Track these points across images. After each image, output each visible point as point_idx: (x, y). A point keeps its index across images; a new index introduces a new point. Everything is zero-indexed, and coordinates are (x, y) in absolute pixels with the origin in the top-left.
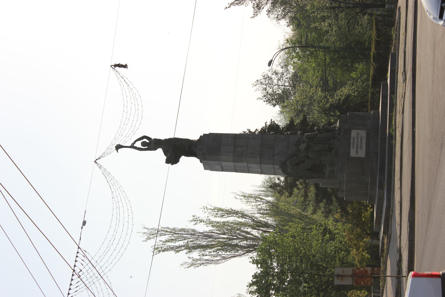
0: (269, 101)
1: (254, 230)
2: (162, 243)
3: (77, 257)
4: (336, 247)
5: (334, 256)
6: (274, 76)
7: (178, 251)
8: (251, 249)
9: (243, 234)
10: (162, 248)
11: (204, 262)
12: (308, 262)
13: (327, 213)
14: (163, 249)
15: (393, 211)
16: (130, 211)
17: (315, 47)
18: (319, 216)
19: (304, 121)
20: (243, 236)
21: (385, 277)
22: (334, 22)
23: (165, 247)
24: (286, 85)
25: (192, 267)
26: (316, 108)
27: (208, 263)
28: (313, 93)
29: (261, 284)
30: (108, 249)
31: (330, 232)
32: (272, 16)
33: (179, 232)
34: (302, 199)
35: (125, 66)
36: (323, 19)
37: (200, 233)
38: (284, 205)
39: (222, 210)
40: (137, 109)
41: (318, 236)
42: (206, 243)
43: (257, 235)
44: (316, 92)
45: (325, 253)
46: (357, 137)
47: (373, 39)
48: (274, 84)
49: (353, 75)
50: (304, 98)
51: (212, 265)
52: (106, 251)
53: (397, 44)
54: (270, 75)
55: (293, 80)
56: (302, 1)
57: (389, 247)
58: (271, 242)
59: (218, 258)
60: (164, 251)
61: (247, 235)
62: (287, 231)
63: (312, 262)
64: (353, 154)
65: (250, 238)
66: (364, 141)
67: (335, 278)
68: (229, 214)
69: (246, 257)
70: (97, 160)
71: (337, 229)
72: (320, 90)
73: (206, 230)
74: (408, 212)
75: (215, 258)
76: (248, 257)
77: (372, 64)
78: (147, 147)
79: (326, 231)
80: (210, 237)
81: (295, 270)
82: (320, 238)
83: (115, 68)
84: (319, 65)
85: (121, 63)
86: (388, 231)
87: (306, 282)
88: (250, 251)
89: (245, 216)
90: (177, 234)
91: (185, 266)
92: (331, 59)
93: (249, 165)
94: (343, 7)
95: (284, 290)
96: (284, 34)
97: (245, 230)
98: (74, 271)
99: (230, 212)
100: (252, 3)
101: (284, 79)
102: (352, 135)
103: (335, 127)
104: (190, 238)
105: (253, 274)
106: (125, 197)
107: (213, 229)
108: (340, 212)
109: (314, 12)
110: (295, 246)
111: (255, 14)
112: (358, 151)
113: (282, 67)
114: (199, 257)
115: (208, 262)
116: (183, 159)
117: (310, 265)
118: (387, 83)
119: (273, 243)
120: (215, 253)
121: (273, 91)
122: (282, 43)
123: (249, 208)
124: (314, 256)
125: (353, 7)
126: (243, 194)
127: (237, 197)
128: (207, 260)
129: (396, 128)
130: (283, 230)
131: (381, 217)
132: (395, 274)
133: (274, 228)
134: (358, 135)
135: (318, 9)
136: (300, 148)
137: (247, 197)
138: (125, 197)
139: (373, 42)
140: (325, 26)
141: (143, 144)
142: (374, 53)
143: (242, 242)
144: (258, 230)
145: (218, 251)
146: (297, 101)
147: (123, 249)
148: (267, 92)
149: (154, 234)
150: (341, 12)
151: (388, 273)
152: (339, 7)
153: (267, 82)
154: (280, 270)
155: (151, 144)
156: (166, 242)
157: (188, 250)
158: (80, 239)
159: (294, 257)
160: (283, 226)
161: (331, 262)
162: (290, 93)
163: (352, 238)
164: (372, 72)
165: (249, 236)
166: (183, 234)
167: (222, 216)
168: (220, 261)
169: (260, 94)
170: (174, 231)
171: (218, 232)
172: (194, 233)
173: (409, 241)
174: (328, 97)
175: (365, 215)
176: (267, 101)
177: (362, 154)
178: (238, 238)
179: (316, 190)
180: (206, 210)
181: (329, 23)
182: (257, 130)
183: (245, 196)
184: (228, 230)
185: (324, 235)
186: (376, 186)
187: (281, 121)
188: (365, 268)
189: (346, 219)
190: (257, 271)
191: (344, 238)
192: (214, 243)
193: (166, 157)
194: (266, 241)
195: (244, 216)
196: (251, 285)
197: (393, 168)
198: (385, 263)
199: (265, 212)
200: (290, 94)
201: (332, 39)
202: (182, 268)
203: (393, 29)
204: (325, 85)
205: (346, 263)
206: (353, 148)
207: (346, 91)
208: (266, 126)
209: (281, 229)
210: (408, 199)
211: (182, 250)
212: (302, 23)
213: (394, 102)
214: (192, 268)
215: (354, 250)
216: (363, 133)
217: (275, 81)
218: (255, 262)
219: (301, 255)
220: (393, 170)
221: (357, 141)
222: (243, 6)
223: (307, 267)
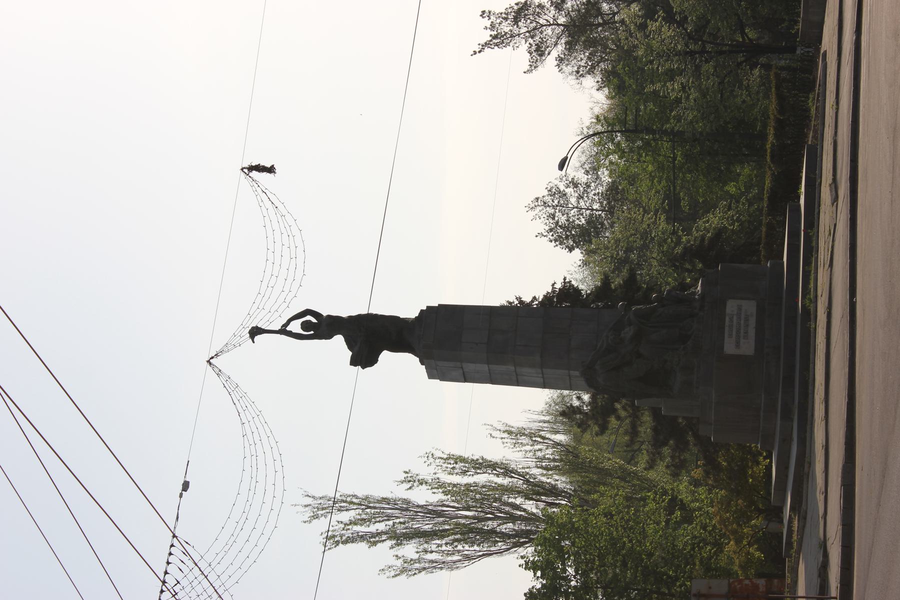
0: (559, 240)
1: (528, 502)
3: (170, 554)
4: (695, 537)
5: (691, 556)
6: (569, 191)
7: (375, 543)
9: (507, 509)
10: (341, 536)
11: (427, 565)
12: (637, 567)
14: (344, 538)
15: (811, 464)
16: (278, 463)
17: (653, 132)
19: (631, 282)
20: (505, 513)
22: (693, 82)
23: (348, 534)
24: (595, 207)
26: (655, 255)
27: (435, 567)
28: (649, 225)
30: (233, 539)
31: (683, 506)
32: (568, 69)
33: (377, 505)
35: (271, 170)
36: (671, 75)
37: (418, 506)
38: (590, 451)
39: (463, 460)
40: (293, 256)
41: (659, 514)
42: (430, 526)
43: (535, 511)
44: (655, 223)
47: (772, 117)
48: (570, 206)
49: (731, 188)
50: (632, 235)
51: (444, 571)
52: (230, 543)
54: (562, 188)
57: (802, 538)
58: (562, 526)
59: (456, 558)
60: (345, 542)
62: (595, 504)
63: (646, 567)
64: (729, 348)
65: (520, 518)
66: (753, 322)
68: (478, 468)
70: (212, 358)
71: (697, 500)
73: (431, 501)
74: (841, 466)
75: (450, 558)
76: (516, 555)
79: (675, 503)
80: (440, 514)
82: (663, 519)
83: (251, 174)
84: (661, 168)
88: (522, 545)
89: (511, 472)
90: (372, 507)
91: (388, 574)
94: (711, 52)
96: (591, 105)
97: (510, 500)
98: (164, 582)
99: (480, 464)
100: (528, 44)
101: (591, 195)
102: (728, 310)
103: (694, 293)
104: (397, 518)
105: (527, 591)
106: (269, 434)
107: (445, 498)
108: (704, 465)
109: (651, 62)
110: (611, 534)
111: (533, 66)
112: (739, 343)
113: (587, 173)
114: (416, 556)
115: (435, 565)
116: (386, 356)
118: (800, 206)
119: (566, 528)
120: (449, 548)
121: (568, 220)
122: (588, 124)
124: (650, 555)
126: (507, 428)
127: (495, 434)
128: (432, 561)
129: (816, 297)
130: (586, 501)
131: (787, 476)
133: (568, 496)
134: (741, 311)
137: (515, 434)
140: (673, 89)
141: (306, 326)
143: (505, 526)
144: (537, 501)
145: (456, 544)
146: (617, 241)
147: (264, 538)
148: (557, 223)
150: (707, 61)
152: (703, 51)
153: (556, 202)
155: (321, 327)
156: (351, 523)
157: (394, 542)
158: (177, 518)
160: (589, 492)
161: (685, 567)
162: (602, 224)
163: (728, 519)
164: (768, 183)
165: (519, 513)
166: (384, 508)
167: (464, 473)
168: (458, 564)
169: (542, 226)
170: (365, 503)
171: (457, 505)
172: (406, 506)
174: (680, 233)
175: (753, 472)
176: (556, 240)
177: (748, 348)
178: (496, 518)
180: (431, 460)
182: (534, 298)
184: (476, 500)
185: (671, 513)
188: (754, 580)
189: (715, 480)
190: (534, 583)
191: (711, 519)
192: (447, 527)
193: (351, 353)
194: (552, 524)
197: (811, 376)
199: (552, 464)
202: (383, 577)
203: (811, 96)
206: (730, 336)
208: (554, 291)
209: (583, 499)
210: (842, 440)
211: (383, 541)
212: (627, 84)
213: (814, 244)
214: (403, 577)
215: (732, 542)
216: (750, 307)
217: (573, 200)
218: (531, 566)
219: (624, 552)
222: (509, 48)
223: (636, 577)
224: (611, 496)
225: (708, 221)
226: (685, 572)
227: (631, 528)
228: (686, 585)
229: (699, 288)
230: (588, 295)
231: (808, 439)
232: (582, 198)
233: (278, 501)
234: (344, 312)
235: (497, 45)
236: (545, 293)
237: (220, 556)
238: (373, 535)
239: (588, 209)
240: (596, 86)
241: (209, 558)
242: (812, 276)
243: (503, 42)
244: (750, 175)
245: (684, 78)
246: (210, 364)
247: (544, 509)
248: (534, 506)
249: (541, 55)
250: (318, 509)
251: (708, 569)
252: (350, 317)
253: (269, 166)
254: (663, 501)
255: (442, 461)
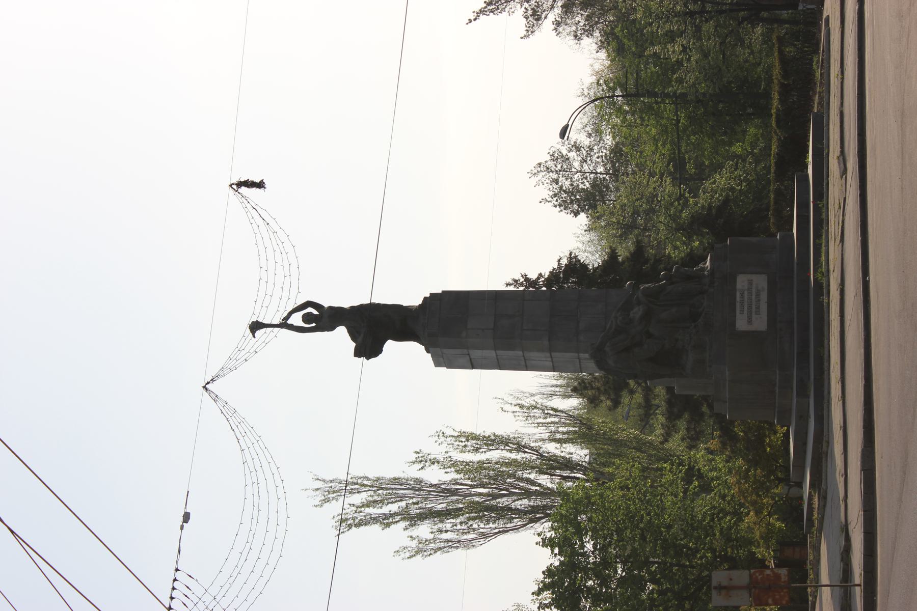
0: (564, 205)
1: (543, 477)
2: (354, 509)
3: (174, 589)
4: (714, 507)
5: (711, 527)
6: (572, 155)
8: (538, 516)
9: (521, 484)
10: (354, 519)
11: (442, 545)
12: (656, 540)
13: (692, 439)
14: (357, 521)
15: (829, 443)
16: (280, 489)
17: (655, 95)
18: (676, 444)
19: (638, 253)
20: (520, 489)
21: (816, 587)
22: (694, 44)
23: (360, 516)
24: (598, 171)
25: (419, 557)
26: (662, 219)
27: (450, 547)
29: (562, 586)
30: (237, 570)
31: (700, 476)
32: (566, 29)
33: (389, 486)
34: (641, 411)
35: (260, 185)
36: (671, 37)
37: (431, 485)
38: (603, 422)
39: (475, 437)
40: (287, 274)
41: (677, 485)
42: (444, 505)
43: (550, 485)
44: (661, 185)
45: (692, 519)
46: (750, 289)
47: (776, 81)
48: (573, 170)
49: (737, 149)
50: (637, 200)
51: (460, 550)
52: (234, 575)
53: (825, 94)
54: (564, 152)
55: (612, 162)
56: (624, 1)
57: (823, 517)
58: (578, 502)
59: (471, 536)
60: (358, 525)
61: (529, 487)
62: (611, 477)
63: (665, 540)
64: (741, 324)
65: (536, 493)
66: (764, 296)
67: (714, 593)
68: (490, 445)
69: (528, 531)
70: (208, 383)
71: (715, 469)
72: (668, 180)
74: (860, 450)
75: (465, 537)
76: (533, 531)
77: (775, 132)
78: (314, 325)
79: (692, 473)
80: (454, 493)
81: (629, 556)
83: (240, 190)
84: (665, 131)
85: (251, 179)
86: (820, 484)
87: (653, 581)
88: (536, 520)
89: (525, 447)
90: (386, 488)
91: (403, 555)
92: (689, 118)
93: (527, 354)
94: (710, 12)
95: (608, 598)
96: (591, 61)
97: (525, 475)
99: (494, 440)
100: (523, 9)
101: (594, 158)
102: (739, 285)
103: (703, 269)
104: (412, 498)
106: (270, 460)
107: (458, 476)
108: (720, 436)
109: (651, 24)
110: (628, 507)
111: (530, 31)
112: (752, 318)
113: (589, 135)
114: (431, 536)
115: (451, 545)
117: (662, 547)
118: (808, 175)
119: (583, 503)
120: (464, 527)
121: (572, 185)
122: (587, 84)
123: (530, 431)
124: (669, 527)
125: (731, 11)
126: (519, 402)
128: (448, 541)
129: (828, 271)
130: (602, 474)
132: (839, 575)
133: (584, 470)
134: (751, 286)
135: (658, 17)
136: (631, 315)
137: (528, 410)
138: (270, 460)
139: (776, 87)
140: (674, 51)
141: (307, 318)
142: (778, 110)
143: (519, 502)
144: (551, 475)
145: (471, 522)
146: (623, 207)
147: (269, 569)
148: (561, 187)
149: (337, 491)
150: (707, 21)
151: (825, 578)
152: (702, 12)
153: (559, 167)
154: (601, 558)
155: (323, 318)
156: (363, 506)
157: (407, 523)
158: (179, 551)
159: (628, 532)
160: (604, 465)
161: (706, 538)
162: (607, 187)
163: (747, 490)
164: (774, 148)
165: (534, 488)
166: (396, 489)
167: (476, 450)
168: (474, 543)
169: (545, 191)
170: (378, 484)
171: (469, 482)
172: (418, 486)
173: (864, 511)
174: (687, 195)
175: (771, 440)
176: (560, 205)
177: (760, 323)
178: (511, 494)
179: (667, 393)
180: (443, 439)
181: (683, 45)
182: (540, 275)
183: (522, 406)
184: (490, 478)
185: (690, 482)
186: (792, 389)
187: (593, 258)
188: (776, 570)
189: (732, 451)
190: (552, 561)
191: (729, 488)
192: (461, 506)
193: (354, 344)
194: (568, 500)
195: (521, 447)
196: (538, 593)
197: (826, 352)
198: (817, 549)
199: (566, 436)
200: (607, 190)
201: (690, 77)
202: (398, 558)
203: (815, 59)
204: (678, 169)
205: (737, 540)
206: (742, 311)
207: (723, 181)
208: (560, 267)
209: (596, 471)
211: (397, 522)
212: (626, 47)
213: (824, 216)
214: (419, 557)
215: (751, 513)
216: (761, 281)
217: (576, 165)
218: (547, 543)
219: (642, 525)
220: (826, 356)
221: (750, 299)
222: (505, 14)
224: (627, 469)
225: (714, 182)
226: (705, 544)
227: (648, 502)
228: (707, 557)
229: (708, 264)
230: (595, 269)
231: (825, 417)
232: (586, 161)
233: (281, 530)
234: (347, 301)
235: (492, 11)
236: (550, 269)
237: (224, 589)
238: (387, 517)
239: (592, 173)
240: (595, 47)
241: (213, 591)
242: (823, 249)
243: (498, 8)
244: (756, 135)
245: (685, 38)
246: (206, 389)
247: (559, 484)
248: (549, 481)
249: (538, 19)
250: (329, 492)
251: (729, 539)
252: (352, 307)
253: (258, 181)
254: (680, 471)
255: (453, 439)
